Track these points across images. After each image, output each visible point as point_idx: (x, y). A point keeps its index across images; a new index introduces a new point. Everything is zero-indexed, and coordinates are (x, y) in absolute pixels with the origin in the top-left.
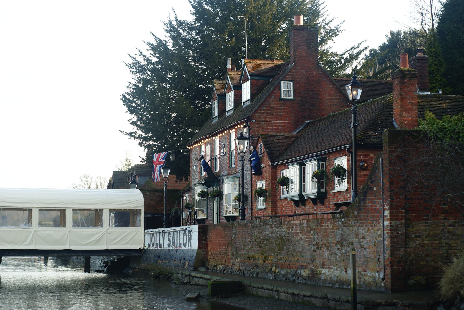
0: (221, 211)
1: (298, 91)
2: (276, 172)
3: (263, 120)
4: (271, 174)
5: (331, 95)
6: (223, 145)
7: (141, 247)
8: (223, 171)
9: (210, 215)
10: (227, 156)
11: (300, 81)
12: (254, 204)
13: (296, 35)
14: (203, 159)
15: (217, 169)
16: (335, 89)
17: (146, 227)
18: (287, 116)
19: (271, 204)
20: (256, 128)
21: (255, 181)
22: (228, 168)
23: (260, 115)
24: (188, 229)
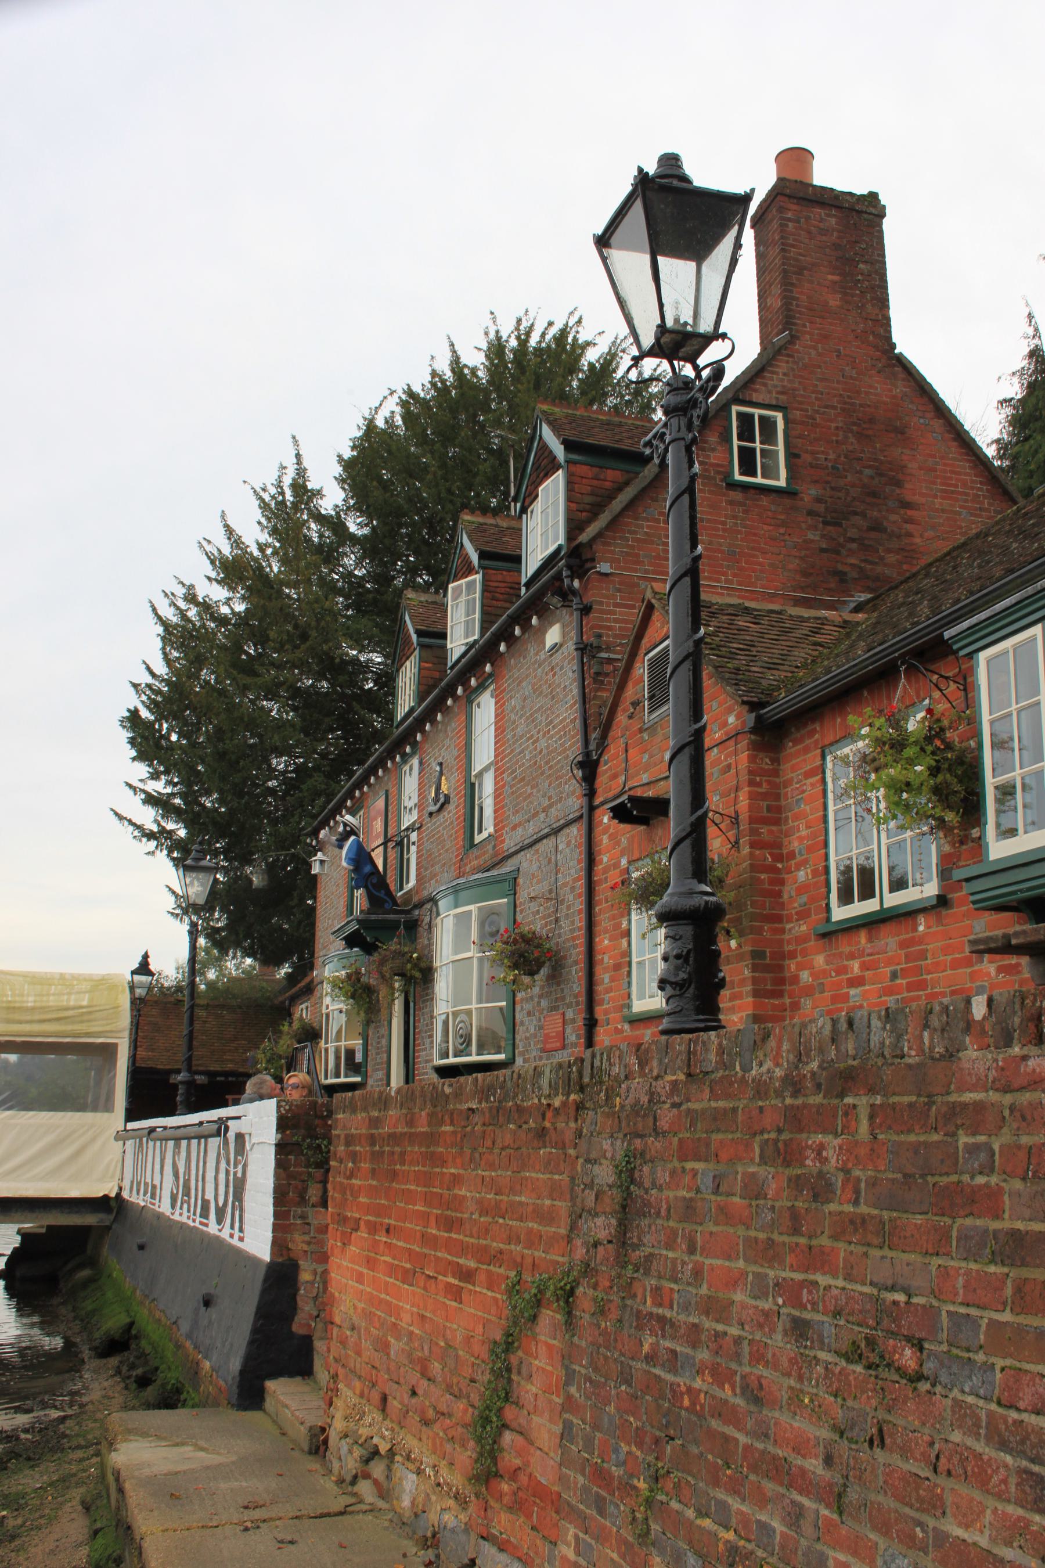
0: (419, 1051)
1: (807, 458)
2: (776, 773)
3: (647, 572)
4: (751, 783)
5: (952, 492)
6: (438, 768)
7: (111, 1191)
8: (435, 875)
9: (378, 1070)
10: (451, 807)
11: (817, 412)
12: (608, 990)
13: (789, 220)
14: (353, 838)
15: (408, 882)
16: (971, 468)
17: (131, 1115)
18: (760, 564)
19: (747, 973)
20: (616, 605)
21: (617, 865)
22: (457, 856)
23: (632, 547)
24: (234, 1126)
